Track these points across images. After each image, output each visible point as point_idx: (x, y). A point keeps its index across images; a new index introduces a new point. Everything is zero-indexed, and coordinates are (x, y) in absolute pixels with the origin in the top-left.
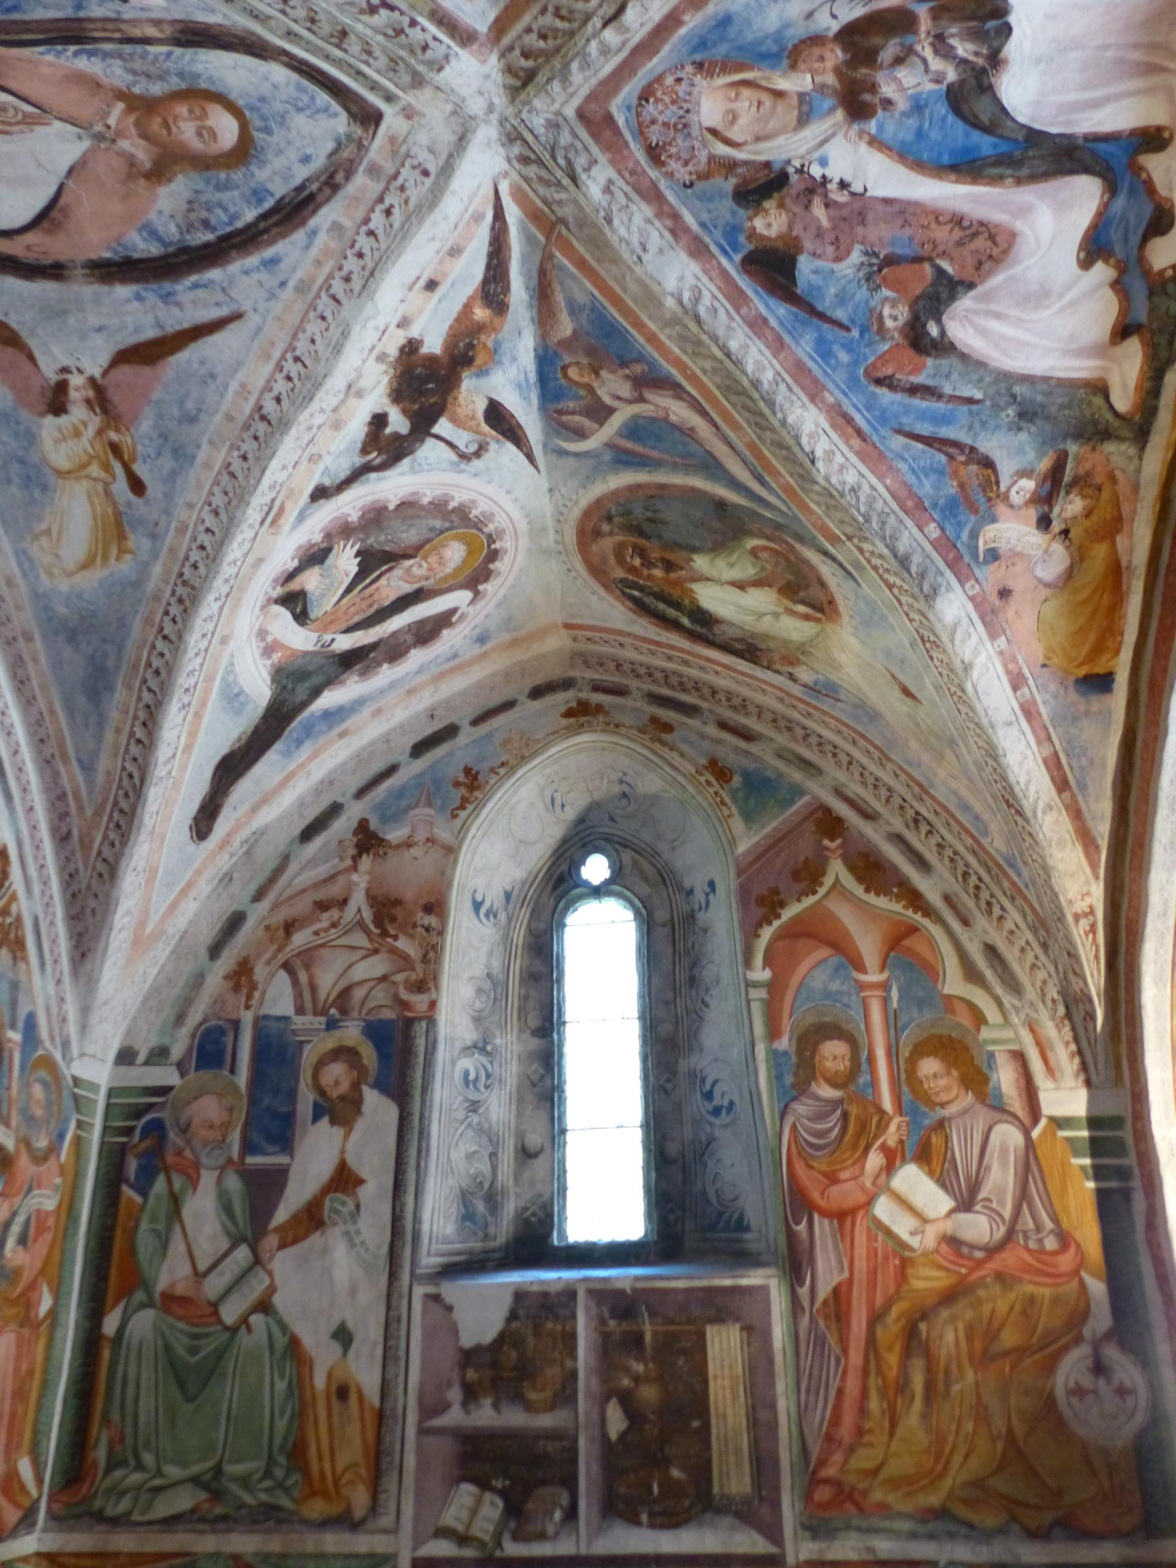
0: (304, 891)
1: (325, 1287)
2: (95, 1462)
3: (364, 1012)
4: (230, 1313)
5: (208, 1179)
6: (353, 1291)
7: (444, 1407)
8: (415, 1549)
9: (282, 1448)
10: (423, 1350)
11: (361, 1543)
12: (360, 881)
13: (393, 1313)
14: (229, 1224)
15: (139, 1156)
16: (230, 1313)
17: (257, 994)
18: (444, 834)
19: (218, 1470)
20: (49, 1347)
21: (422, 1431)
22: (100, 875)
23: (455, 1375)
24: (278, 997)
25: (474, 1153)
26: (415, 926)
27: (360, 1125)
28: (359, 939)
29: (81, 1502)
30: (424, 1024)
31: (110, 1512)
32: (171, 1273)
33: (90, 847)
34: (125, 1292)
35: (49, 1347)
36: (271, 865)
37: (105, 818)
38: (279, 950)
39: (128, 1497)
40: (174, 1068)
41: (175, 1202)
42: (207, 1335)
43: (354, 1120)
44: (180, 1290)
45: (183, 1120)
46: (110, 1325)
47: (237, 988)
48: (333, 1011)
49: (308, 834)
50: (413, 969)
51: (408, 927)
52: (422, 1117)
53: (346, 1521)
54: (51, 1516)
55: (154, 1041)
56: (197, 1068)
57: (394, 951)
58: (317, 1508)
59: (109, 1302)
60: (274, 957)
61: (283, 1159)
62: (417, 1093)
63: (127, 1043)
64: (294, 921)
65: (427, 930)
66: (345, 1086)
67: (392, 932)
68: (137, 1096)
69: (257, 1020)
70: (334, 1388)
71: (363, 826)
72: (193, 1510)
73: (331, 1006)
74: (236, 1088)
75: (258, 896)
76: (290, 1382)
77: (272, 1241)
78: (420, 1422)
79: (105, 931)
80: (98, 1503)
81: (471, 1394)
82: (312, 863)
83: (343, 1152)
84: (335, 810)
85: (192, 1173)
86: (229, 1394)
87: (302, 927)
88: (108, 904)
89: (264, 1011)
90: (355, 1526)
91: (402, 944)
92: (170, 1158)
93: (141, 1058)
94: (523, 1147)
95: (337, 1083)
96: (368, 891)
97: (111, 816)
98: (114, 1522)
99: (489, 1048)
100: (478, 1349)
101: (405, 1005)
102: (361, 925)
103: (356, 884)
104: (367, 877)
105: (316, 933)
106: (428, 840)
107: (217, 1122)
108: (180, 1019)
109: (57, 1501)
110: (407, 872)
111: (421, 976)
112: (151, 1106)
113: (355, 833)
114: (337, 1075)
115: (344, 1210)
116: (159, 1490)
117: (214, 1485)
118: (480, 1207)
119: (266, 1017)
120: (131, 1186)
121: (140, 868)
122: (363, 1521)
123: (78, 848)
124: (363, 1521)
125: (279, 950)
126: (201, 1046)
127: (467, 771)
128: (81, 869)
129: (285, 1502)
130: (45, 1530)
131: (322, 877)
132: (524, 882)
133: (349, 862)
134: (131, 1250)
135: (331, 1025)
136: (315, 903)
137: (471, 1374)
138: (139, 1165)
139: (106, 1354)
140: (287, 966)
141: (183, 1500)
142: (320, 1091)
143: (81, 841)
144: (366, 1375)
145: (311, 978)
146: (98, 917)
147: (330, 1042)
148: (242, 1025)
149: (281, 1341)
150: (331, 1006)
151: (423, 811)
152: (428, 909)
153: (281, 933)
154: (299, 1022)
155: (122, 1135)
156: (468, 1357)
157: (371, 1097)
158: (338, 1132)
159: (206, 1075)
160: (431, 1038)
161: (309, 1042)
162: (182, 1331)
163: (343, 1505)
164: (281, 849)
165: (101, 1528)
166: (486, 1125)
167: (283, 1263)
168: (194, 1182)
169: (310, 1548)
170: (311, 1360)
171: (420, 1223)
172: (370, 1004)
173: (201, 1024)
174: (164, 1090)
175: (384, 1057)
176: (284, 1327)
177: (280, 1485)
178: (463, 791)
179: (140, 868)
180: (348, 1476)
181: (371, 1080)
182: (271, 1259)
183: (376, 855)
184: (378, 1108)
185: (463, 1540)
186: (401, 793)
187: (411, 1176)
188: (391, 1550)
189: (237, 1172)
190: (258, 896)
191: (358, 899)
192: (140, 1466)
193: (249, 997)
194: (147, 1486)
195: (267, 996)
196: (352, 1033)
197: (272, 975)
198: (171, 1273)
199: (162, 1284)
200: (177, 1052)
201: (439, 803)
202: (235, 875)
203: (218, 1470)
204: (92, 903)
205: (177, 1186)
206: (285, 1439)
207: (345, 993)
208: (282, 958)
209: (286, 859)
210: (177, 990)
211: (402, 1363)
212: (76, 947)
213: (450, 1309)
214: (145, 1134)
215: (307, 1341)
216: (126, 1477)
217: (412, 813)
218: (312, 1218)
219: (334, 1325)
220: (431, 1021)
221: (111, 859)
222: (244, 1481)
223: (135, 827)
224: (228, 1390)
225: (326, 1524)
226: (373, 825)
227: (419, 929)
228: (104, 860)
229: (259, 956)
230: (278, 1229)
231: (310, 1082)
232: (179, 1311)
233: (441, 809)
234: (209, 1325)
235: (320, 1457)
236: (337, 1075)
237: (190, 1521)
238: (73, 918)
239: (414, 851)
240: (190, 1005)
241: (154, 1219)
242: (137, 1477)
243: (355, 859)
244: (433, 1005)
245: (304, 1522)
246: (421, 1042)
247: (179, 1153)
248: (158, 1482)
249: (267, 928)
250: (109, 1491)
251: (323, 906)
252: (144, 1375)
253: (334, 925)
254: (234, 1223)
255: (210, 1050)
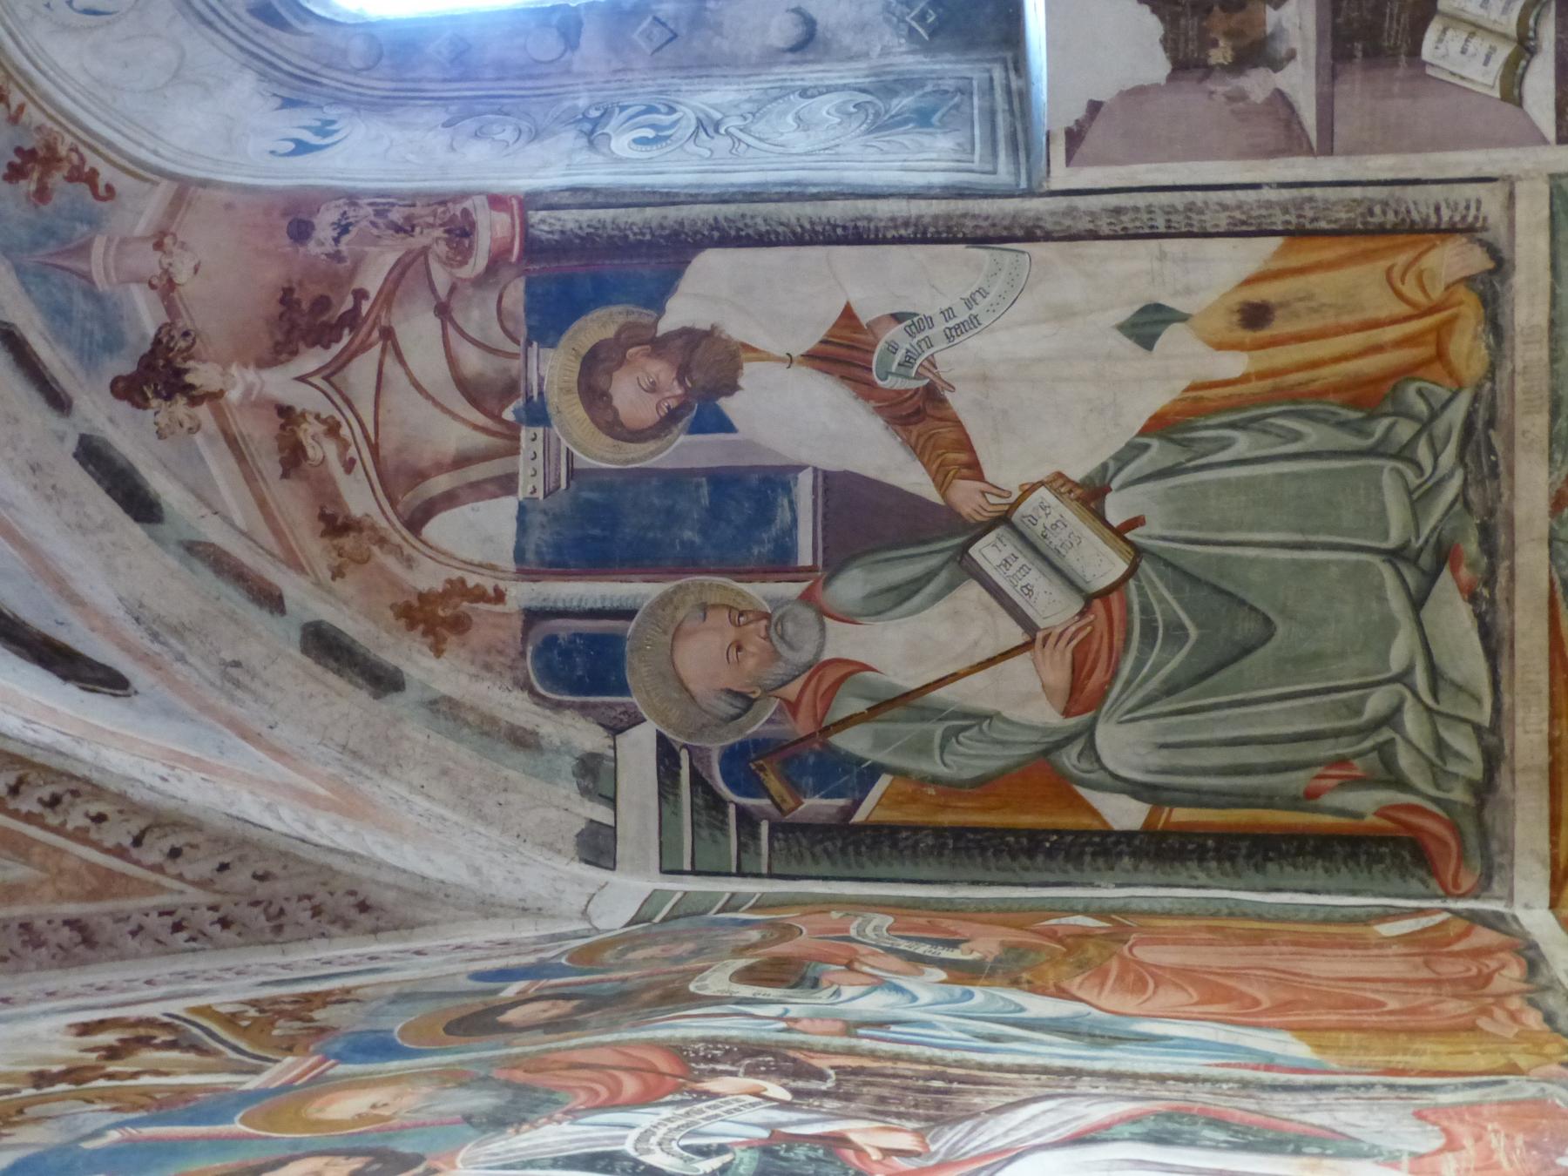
0: (262, 504)
1: (1056, 373)
2: (1382, 813)
3: (511, 347)
4: (1102, 564)
5: (843, 642)
6: (1062, 314)
7: (1280, 98)
8: (1544, 141)
9: (1358, 429)
10: (1173, 158)
11: (1531, 249)
12: (240, 383)
13: (1104, 227)
14: (930, 589)
15: (798, 792)
16: (1102, 564)
17: (472, 580)
18: (142, 211)
19: (1395, 556)
20: (1168, 914)
21: (1327, 147)
22: (175, 853)
23: (1221, 87)
24: (478, 533)
25: (798, 118)
26: (337, 257)
27: (737, 329)
28: (362, 372)
29: (1455, 828)
30: (535, 217)
31: (1476, 771)
32: (1027, 698)
33: (110, 873)
34: (1062, 789)
35: (1168, 914)
36: (206, 576)
37: (33, 831)
38: (382, 541)
39: (1447, 736)
40: (620, 739)
41: (894, 704)
42: (1146, 609)
43: (728, 342)
44: (1059, 676)
45: (725, 707)
46: (1125, 814)
47: (460, 625)
48: (508, 415)
49: (139, 504)
50: (425, 251)
51: (340, 271)
52: (722, 199)
53: (1490, 287)
54: (1482, 888)
55: (567, 789)
56: (623, 689)
57: (388, 296)
58: (1468, 348)
59: (1086, 822)
60: (397, 551)
61: (805, 482)
62: (673, 213)
63: (570, 846)
64: (323, 517)
65: (344, 229)
66: (661, 371)
67: (349, 303)
68: (677, 813)
69: (526, 572)
70: (1248, 336)
71: (129, 390)
72: (1473, 598)
73: (497, 418)
74: (665, 601)
75: (271, 600)
76: (1232, 425)
77: (967, 498)
78: (1310, 152)
79: (304, 852)
80: (1459, 795)
81: (1257, 53)
82: (202, 494)
83: (790, 360)
84: (93, 455)
85: (832, 675)
86: (1258, 553)
87: (336, 498)
88: (244, 842)
89: (508, 562)
90: (1501, 265)
91: (372, 281)
92: (802, 726)
93: (602, 814)
94: (793, 50)
95: (653, 388)
96: (262, 364)
97: (29, 818)
98: (1493, 759)
99: (594, 114)
100: (1171, 44)
101: (497, 261)
102: (332, 372)
103: (248, 391)
104: (234, 370)
105: (349, 466)
106: (159, 246)
107: (731, 634)
108: (522, 740)
109: (1456, 885)
110: (224, 281)
111: (439, 232)
112: (697, 779)
113: (141, 403)
114: (637, 392)
115: (905, 344)
116: (1434, 672)
117: (1426, 560)
118: (904, 102)
119: (519, 555)
120: (857, 804)
121: (164, 771)
122: (1492, 251)
123: (109, 905)
124: (1492, 251)
125: (382, 541)
126: (577, 688)
127: (15, 173)
128: (164, 900)
129: (1457, 413)
130: (1510, 898)
131: (232, 462)
132: (263, 76)
133: (203, 412)
134: (982, 784)
135: (537, 414)
136: (285, 475)
137: (1220, 54)
138: (816, 791)
139: (1181, 815)
140: (415, 523)
141: (1453, 617)
142: (671, 419)
143: (94, 895)
144: (1218, 271)
145: (440, 468)
146: (275, 868)
147: (570, 413)
148: (535, 604)
149: (1158, 453)
150: (497, 418)
151: (98, 263)
152: (301, 231)
153: (348, 542)
154: (530, 483)
155: (755, 836)
156: (1187, 63)
157: (680, 312)
158: (751, 373)
159: (637, 671)
160: (566, 198)
161: (570, 457)
162: (1139, 664)
163: (1462, 293)
164: (173, 563)
165: (1503, 778)
166: (747, 107)
167: (1007, 466)
168: (853, 668)
169: (1541, 353)
170: (1193, 388)
171: (930, 187)
172: (496, 336)
173: (532, 692)
174: (666, 753)
175: (601, 295)
176: (1133, 450)
177: (1426, 425)
178: (57, 179)
179: (164, 771)
180: (1410, 289)
181: (643, 316)
182: (1001, 492)
183: (188, 353)
184: (706, 294)
185: (1525, 47)
186: (58, 314)
187: (837, 210)
188: (1544, 188)
189: (828, 581)
190: (271, 600)
191: (280, 383)
192: (1391, 718)
193: (479, 595)
194: (1429, 700)
195: (477, 558)
196: (553, 369)
197: (439, 554)
198: (1027, 698)
199: (1047, 715)
200: (589, 737)
201: (82, 229)
202: (228, 656)
203: (1395, 556)
204: (240, 878)
205: (860, 706)
206: (1342, 425)
207: (471, 390)
208: (397, 533)
209: (197, 550)
210: (464, 753)
211: (1199, 196)
212: (347, 925)
213: (1095, 107)
214: (749, 784)
215: (1158, 399)
216: (1409, 742)
217: (102, 285)
218: (920, 413)
219: (1127, 346)
220: (531, 201)
221: (135, 826)
222: (1418, 500)
223: (55, 762)
224: (1251, 552)
225: (1496, 327)
226: (125, 365)
227: (343, 247)
228: (137, 842)
229: (394, 583)
230: (942, 487)
231: (651, 446)
232: (1099, 676)
233: (94, 222)
234: (1127, 609)
235: (1378, 349)
236: (637, 392)
237: (1492, 602)
238: (279, 929)
239: (182, 275)
240: (493, 721)
241: (921, 748)
242: (1412, 722)
243: (195, 397)
244: (497, 201)
245: (1492, 370)
246: (572, 219)
247: (793, 707)
248: (1420, 679)
249: (338, 573)
250: (1438, 775)
251: (293, 458)
252: (1221, 734)
253: (333, 429)
254: (930, 576)
255: (584, 666)
